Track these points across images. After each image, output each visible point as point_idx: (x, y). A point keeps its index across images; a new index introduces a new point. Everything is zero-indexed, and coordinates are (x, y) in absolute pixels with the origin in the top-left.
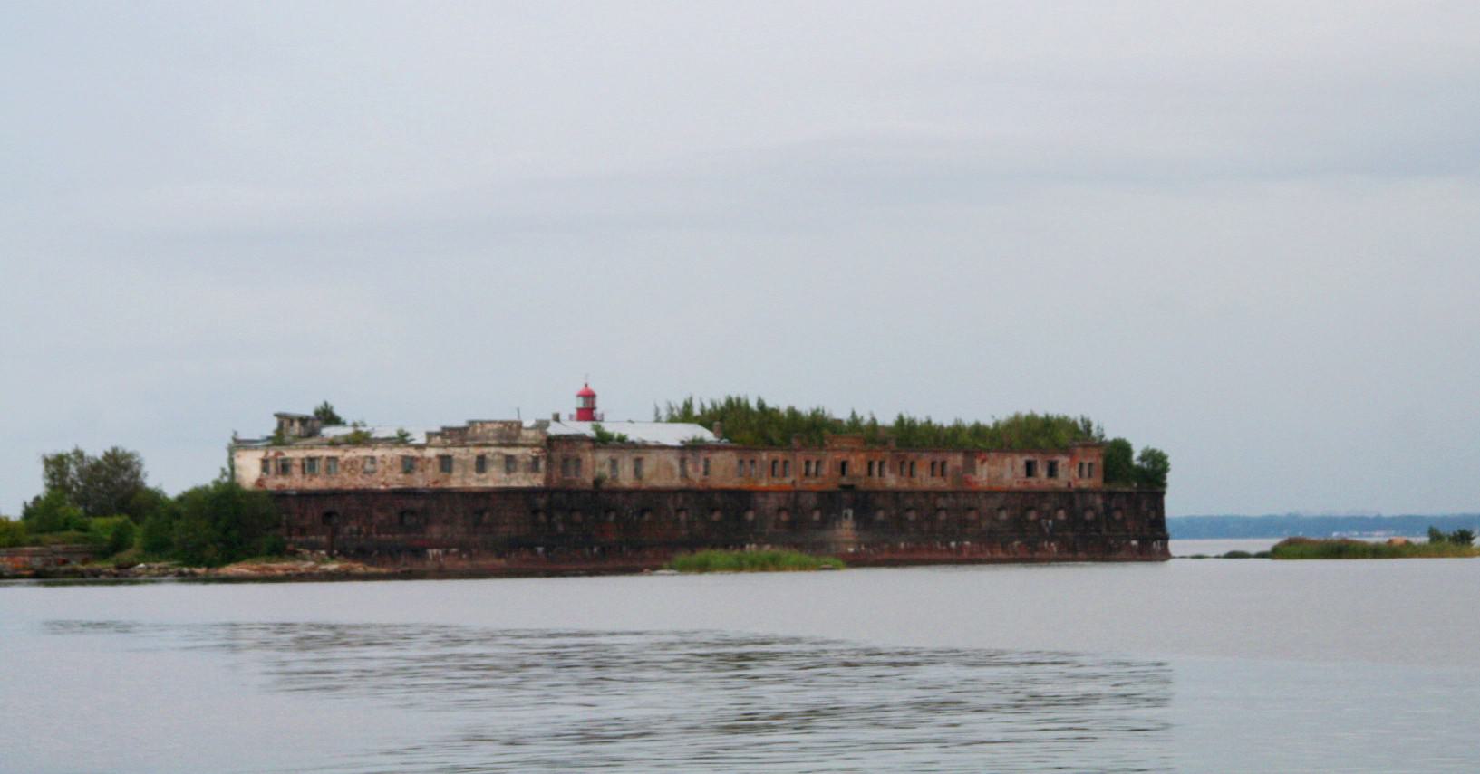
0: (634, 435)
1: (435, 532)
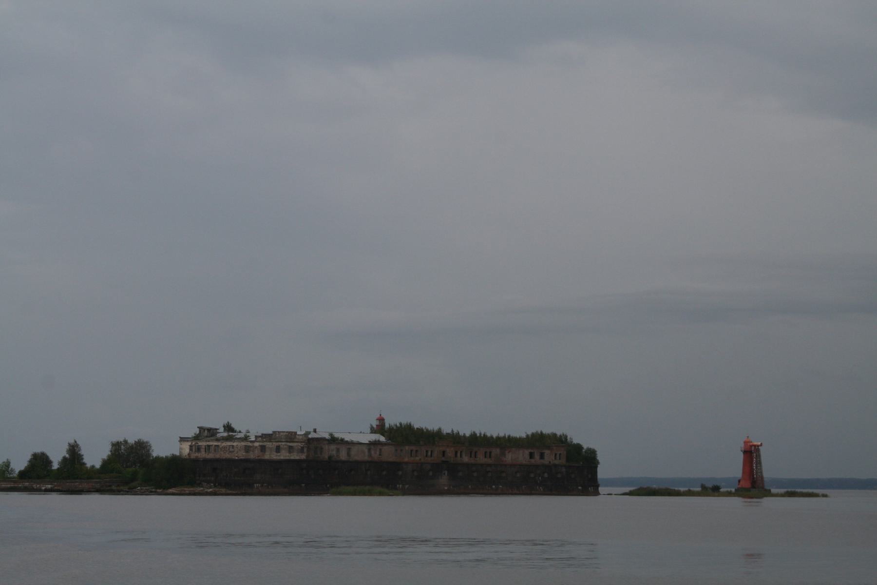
0: (347, 438)
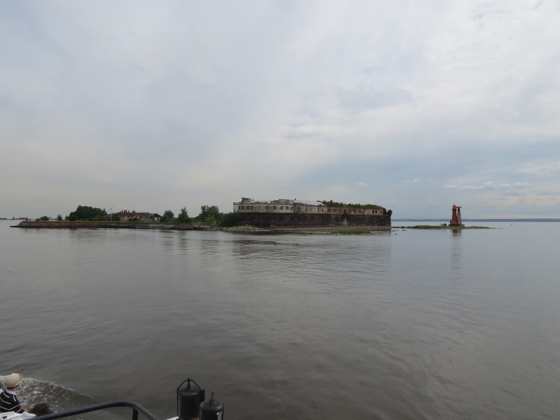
1: (272, 221)
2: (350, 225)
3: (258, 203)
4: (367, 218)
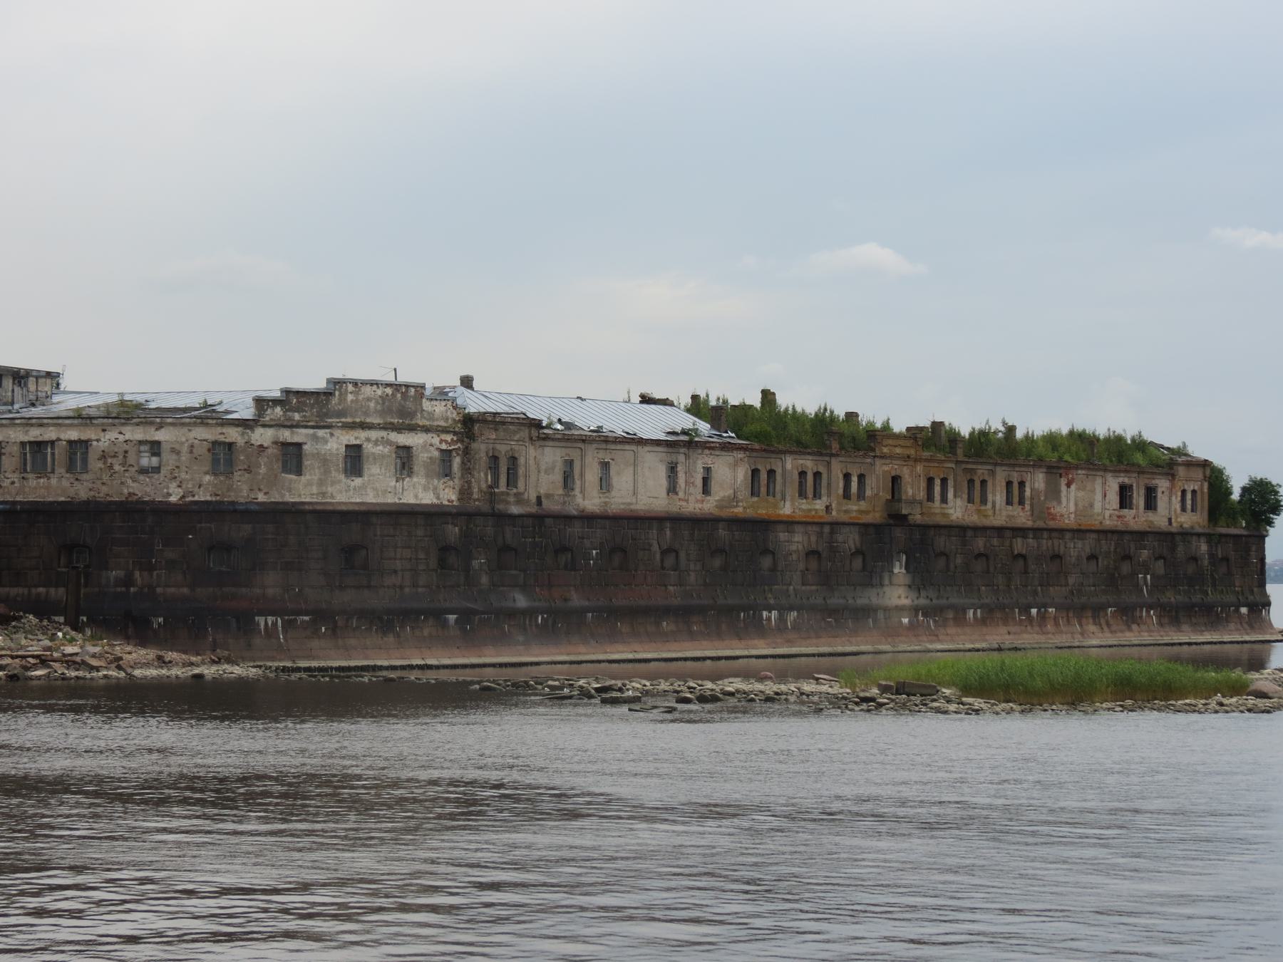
1: (271, 583)
2: (935, 614)
3: (126, 412)
4: (1075, 549)
